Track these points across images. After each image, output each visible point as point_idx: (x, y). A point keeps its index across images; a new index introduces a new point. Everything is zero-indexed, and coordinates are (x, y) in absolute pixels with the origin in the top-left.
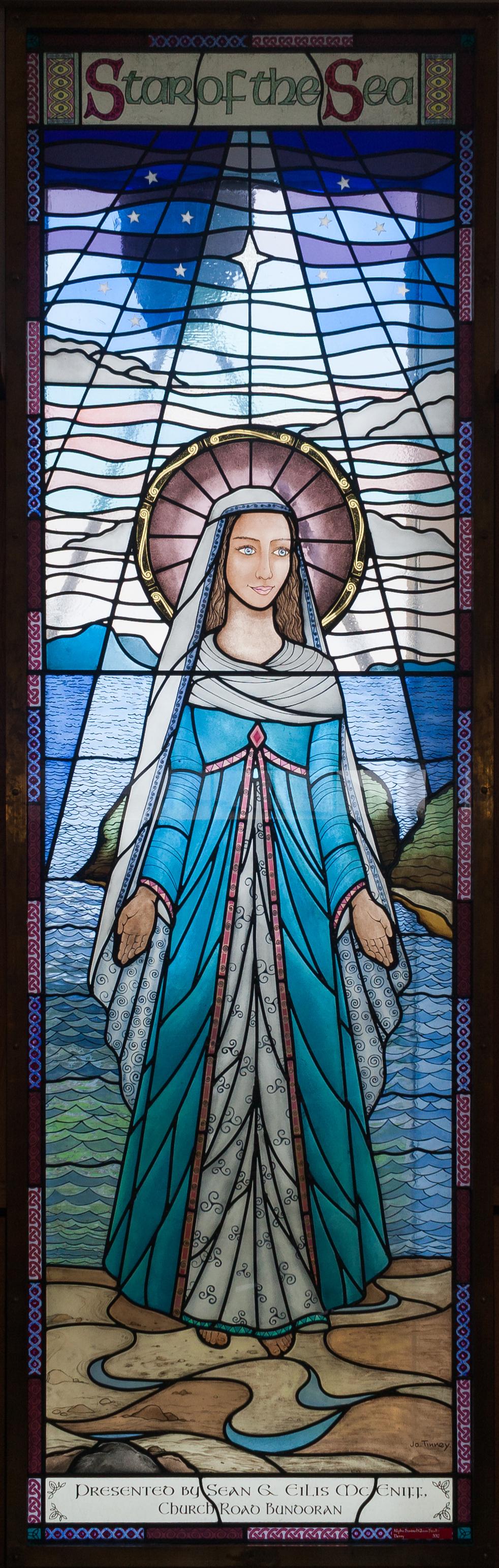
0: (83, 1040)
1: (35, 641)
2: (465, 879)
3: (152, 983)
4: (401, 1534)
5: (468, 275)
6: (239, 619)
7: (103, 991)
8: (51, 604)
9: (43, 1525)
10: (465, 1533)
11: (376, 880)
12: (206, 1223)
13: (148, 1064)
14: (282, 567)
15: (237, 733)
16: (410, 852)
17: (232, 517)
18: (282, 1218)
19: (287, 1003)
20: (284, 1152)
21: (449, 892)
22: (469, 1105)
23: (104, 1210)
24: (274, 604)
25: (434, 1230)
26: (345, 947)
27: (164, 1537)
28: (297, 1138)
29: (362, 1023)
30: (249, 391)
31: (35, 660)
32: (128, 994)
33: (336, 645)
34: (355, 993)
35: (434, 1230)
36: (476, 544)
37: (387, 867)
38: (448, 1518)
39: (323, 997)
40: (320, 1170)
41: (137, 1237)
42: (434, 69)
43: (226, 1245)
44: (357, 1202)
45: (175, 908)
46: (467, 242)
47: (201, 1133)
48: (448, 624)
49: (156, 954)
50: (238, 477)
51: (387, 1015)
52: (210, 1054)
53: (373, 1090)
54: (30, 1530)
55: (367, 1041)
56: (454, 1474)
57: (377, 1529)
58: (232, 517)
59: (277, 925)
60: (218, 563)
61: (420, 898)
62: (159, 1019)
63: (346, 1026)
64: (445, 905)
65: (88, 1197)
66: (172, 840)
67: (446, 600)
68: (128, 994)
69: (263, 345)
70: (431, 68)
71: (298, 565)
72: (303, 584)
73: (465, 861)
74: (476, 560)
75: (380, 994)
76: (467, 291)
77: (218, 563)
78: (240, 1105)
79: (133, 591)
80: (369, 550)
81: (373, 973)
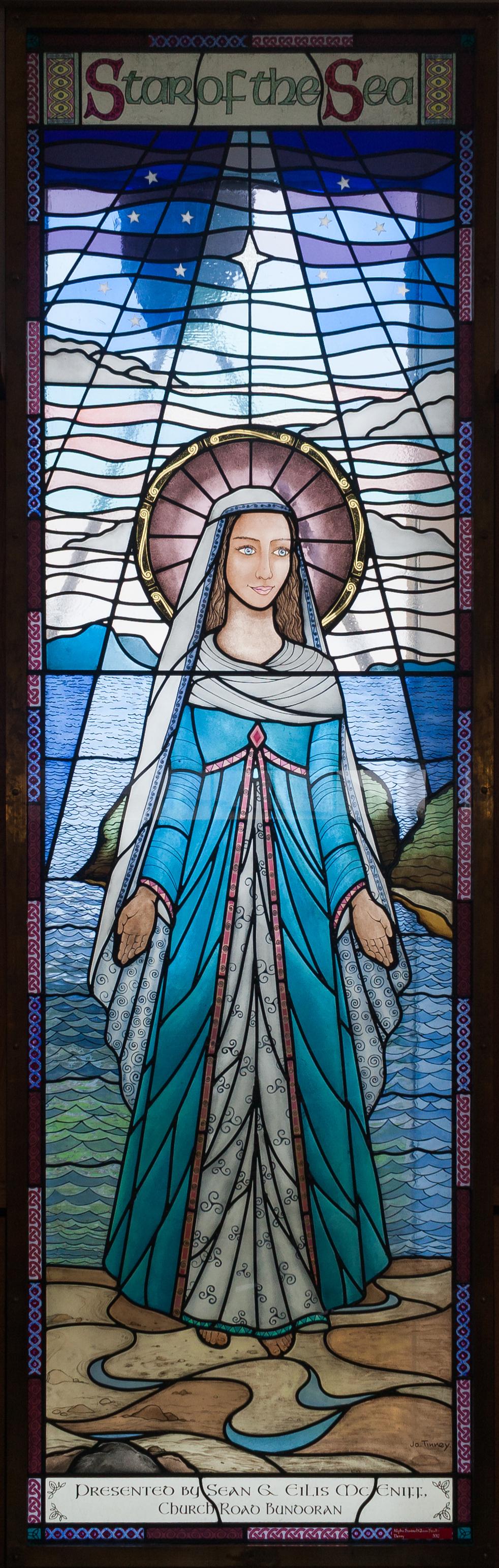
0: (83, 1040)
1: (35, 641)
2: (465, 879)
3: (152, 983)
4: (401, 1534)
5: (468, 275)
6: (239, 619)
7: (103, 991)
8: (51, 604)
9: (43, 1525)
10: (465, 1533)
11: (376, 880)
12: (206, 1223)
13: (148, 1064)
14: (282, 567)
15: (237, 733)
16: (410, 852)
17: (232, 517)
18: (282, 1218)
19: (287, 1003)
20: (284, 1152)
21: (449, 892)
22: (469, 1105)
23: (104, 1210)
24: (274, 604)
25: (434, 1230)
26: (345, 947)
27: (164, 1537)
28: (297, 1138)
29: (362, 1023)
30: (249, 391)
31: (35, 660)
32: (128, 994)
33: (336, 645)
34: (355, 993)
35: (434, 1230)
36: (476, 544)
37: (387, 867)
38: (448, 1518)
39: (323, 997)
40: (320, 1170)
41: (137, 1237)
42: (434, 69)
43: (226, 1245)
44: (357, 1202)
45: (175, 908)
46: (467, 242)
47: (201, 1133)
48: (448, 624)
49: (156, 954)
50: (238, 477)
51: (387, 1015)
52: (210, 1054)
53: (373, 1090)
54: (30, 1530)
55: (367, 1041)
56: (454, 1474)
57: (377, 1529)
58: (232, 517)
59: (277, 925)
60: (218, 563)
61: (420, 898)
62: (159, 1019)
63: (346, 1026)
64: (445, 905)
65: (88, 1197)
66: (172, 840)
67: (446, 600)
68: (128, 994)
69: (263, 345)
70: (431, 68)
71: (298, 565)
72: (303, 584)
73: (465, 861)
74: (476, 560)
75: (380, 994)
76: (467, 291)
77: (218, 563)
78: (240, 1105)
79: (133, 591)
80: (369, 550)
81: (373, 973)
